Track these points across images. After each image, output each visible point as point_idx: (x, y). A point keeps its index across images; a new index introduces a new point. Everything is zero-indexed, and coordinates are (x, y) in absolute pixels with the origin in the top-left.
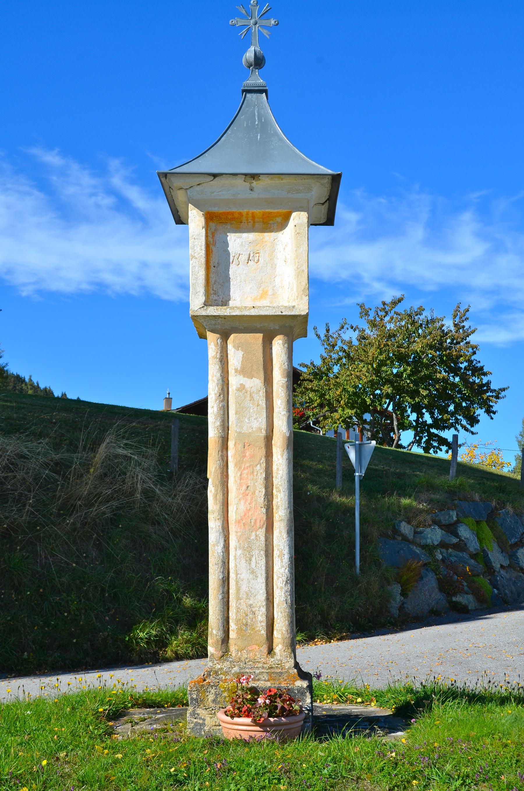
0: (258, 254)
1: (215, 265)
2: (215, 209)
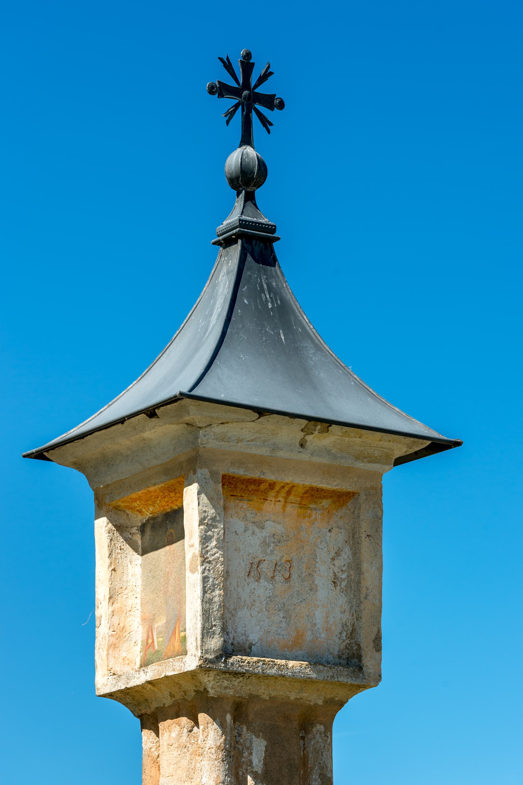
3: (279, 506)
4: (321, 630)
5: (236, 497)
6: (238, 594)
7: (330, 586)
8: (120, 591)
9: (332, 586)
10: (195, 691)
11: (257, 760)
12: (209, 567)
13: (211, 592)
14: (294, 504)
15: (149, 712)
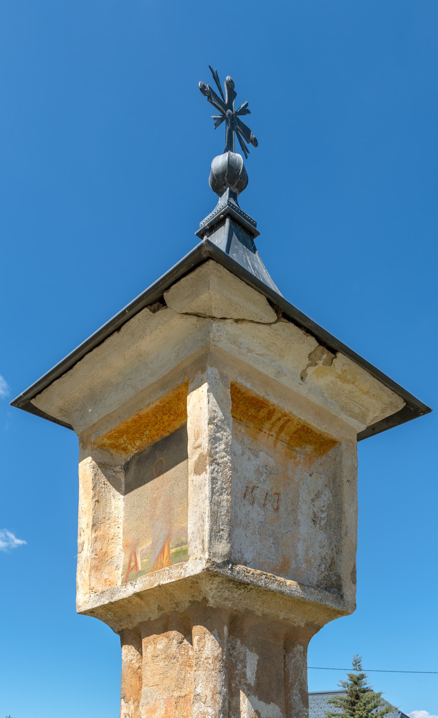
3: (271, 440)
4: (302, 562)
6: (235, 513)
7: (310, 523)
8: (103, 520)
9: (312, 524)
10: (190, 601)
11: (250, 673)
12: (218, 469)
13: (220, 495)
15: (130, 627)
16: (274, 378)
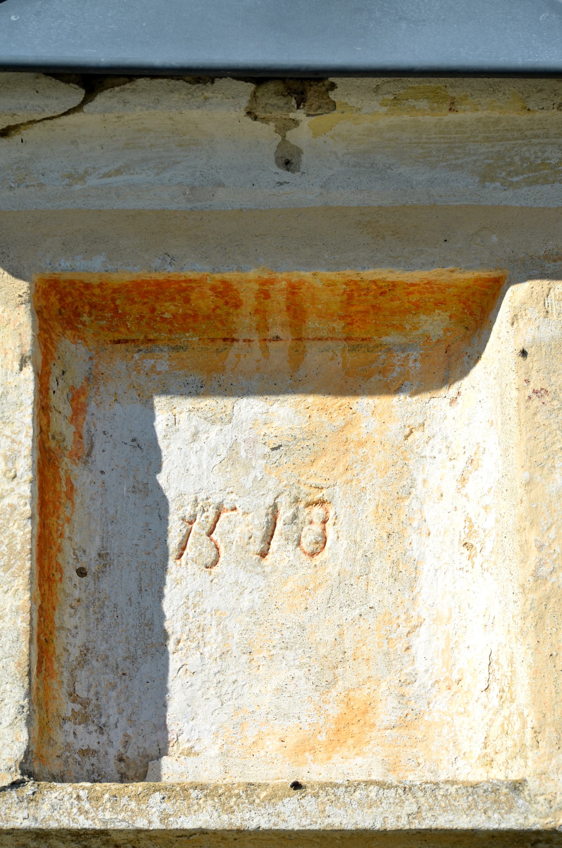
0: (317, 511)
1: (84, 562)
2: (91, 267)
5: (131, 346)
14: (329, 343)
16: (190, 206)
